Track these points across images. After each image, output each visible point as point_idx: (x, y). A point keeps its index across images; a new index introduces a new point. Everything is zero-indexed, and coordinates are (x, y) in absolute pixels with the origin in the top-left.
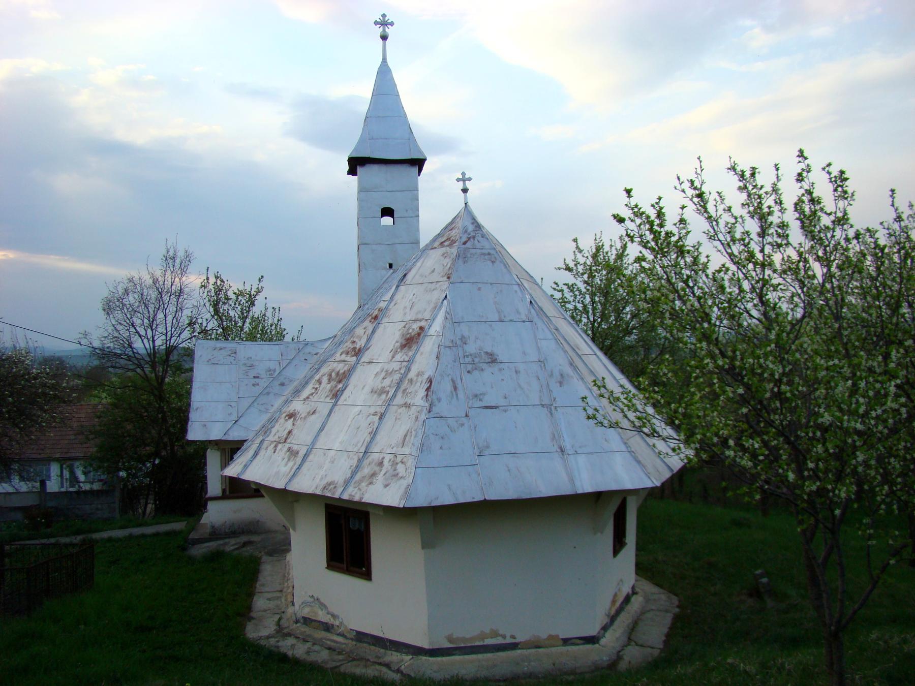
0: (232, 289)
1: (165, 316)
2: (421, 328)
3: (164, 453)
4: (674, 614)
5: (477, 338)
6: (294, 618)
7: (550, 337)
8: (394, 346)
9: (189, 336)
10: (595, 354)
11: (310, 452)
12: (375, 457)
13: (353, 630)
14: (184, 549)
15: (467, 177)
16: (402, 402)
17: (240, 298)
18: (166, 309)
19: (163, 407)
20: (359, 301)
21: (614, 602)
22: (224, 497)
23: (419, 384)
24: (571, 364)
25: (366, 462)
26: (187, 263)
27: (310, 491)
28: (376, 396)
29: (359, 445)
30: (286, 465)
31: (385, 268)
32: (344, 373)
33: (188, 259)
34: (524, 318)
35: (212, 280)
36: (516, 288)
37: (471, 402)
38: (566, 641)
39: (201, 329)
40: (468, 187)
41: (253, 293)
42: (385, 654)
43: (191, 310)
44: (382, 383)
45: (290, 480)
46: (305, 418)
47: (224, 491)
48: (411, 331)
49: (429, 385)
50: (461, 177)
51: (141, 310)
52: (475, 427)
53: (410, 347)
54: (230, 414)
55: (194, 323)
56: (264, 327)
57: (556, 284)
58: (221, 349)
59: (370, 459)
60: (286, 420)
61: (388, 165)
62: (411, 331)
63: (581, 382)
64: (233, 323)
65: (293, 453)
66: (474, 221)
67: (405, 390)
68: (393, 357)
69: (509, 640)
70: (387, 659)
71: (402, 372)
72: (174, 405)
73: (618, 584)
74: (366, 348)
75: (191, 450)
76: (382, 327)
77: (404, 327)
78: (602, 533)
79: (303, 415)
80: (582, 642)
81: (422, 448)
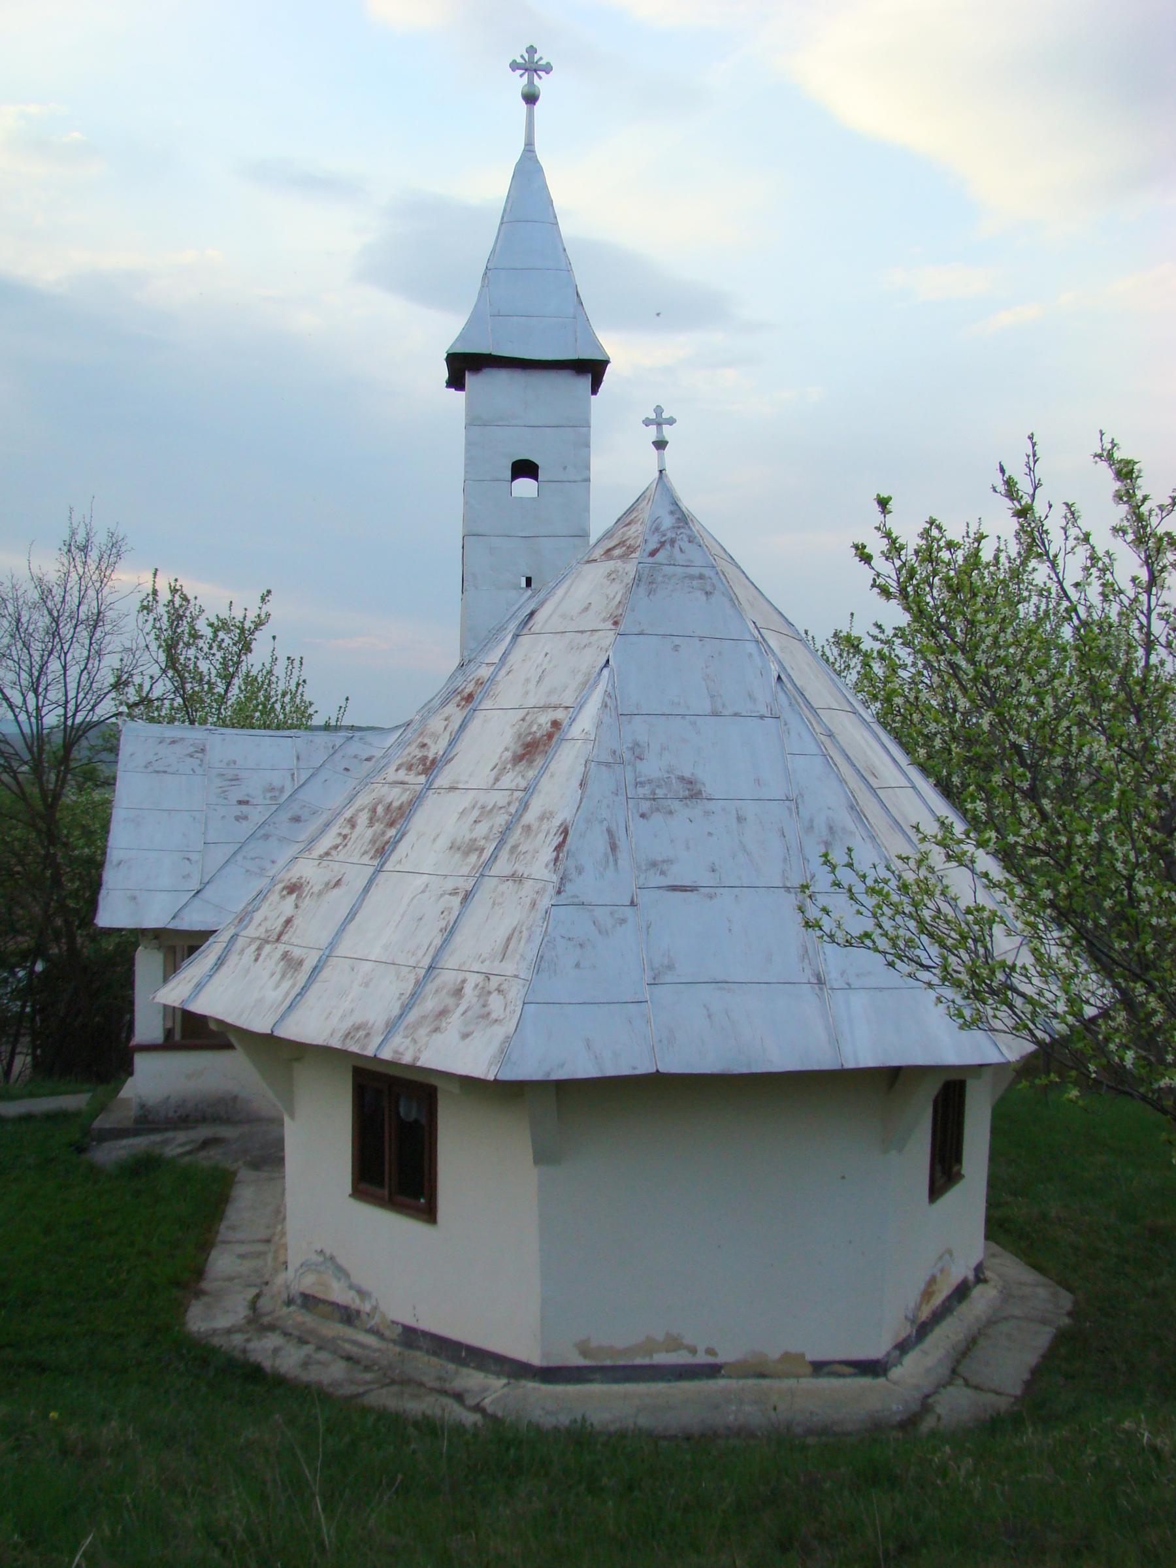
4: (1057, 1329)
5: (664, 748)
6: (285, 1296)
7: (815, 750)
8: (501, 757)
10: (914, 787)
11: (325, 962)
12: (448, 978)
13: (397, 1324)
14: (81, 1149)
16: (508, 871)
17: (221, 635)
18: (66, 654)
19: (55, 855)
20: (463, 647)
21: (927, 1294)
24: (852, 807)
25: (431, 987)
26: (112, 559)
27: (319, 1040)
28: (458, 856)
29: (420, 953)
30: (277, 986)
31: (517, 587)
32: (400, 807)
33: (114, 551)
34: (764, 711)
36: (751, 647)
37: (642, 877)
38: (819, 1368)
39: (140, 696)
40: (667, 439)
41: (248, 625)
43: (119, 656)
44: (471, 830)
45: (283, 1017)
46: (320, 894)
47: (169, 1033)
48: (534, 728)
49: (561, 839)
50: (653, 416)
51: (14, 653)
52: (648, 927)
53: (531, 762)
54: (187, 876)
55: (126, 683)
56: (268, 698)
57: (879, 627)
58: (173, 742)
59: (438, 981)
60: (283, 897)
61: (528, 371)
62: (534, 728)
63: (869, 845)
64: (206, 687)
65: (291, 963)
66: (675, 507)
67: (514, 848)
68: (497, 779)
69: (702, 1358)
70: (458, 1384)
71: (512, 809)
72: (76, 852)
74: (446, 758)
75: (109, 945)
76: (480, 716)
77: (523, 720)
79: (316, 889)
80: (851, 1370)
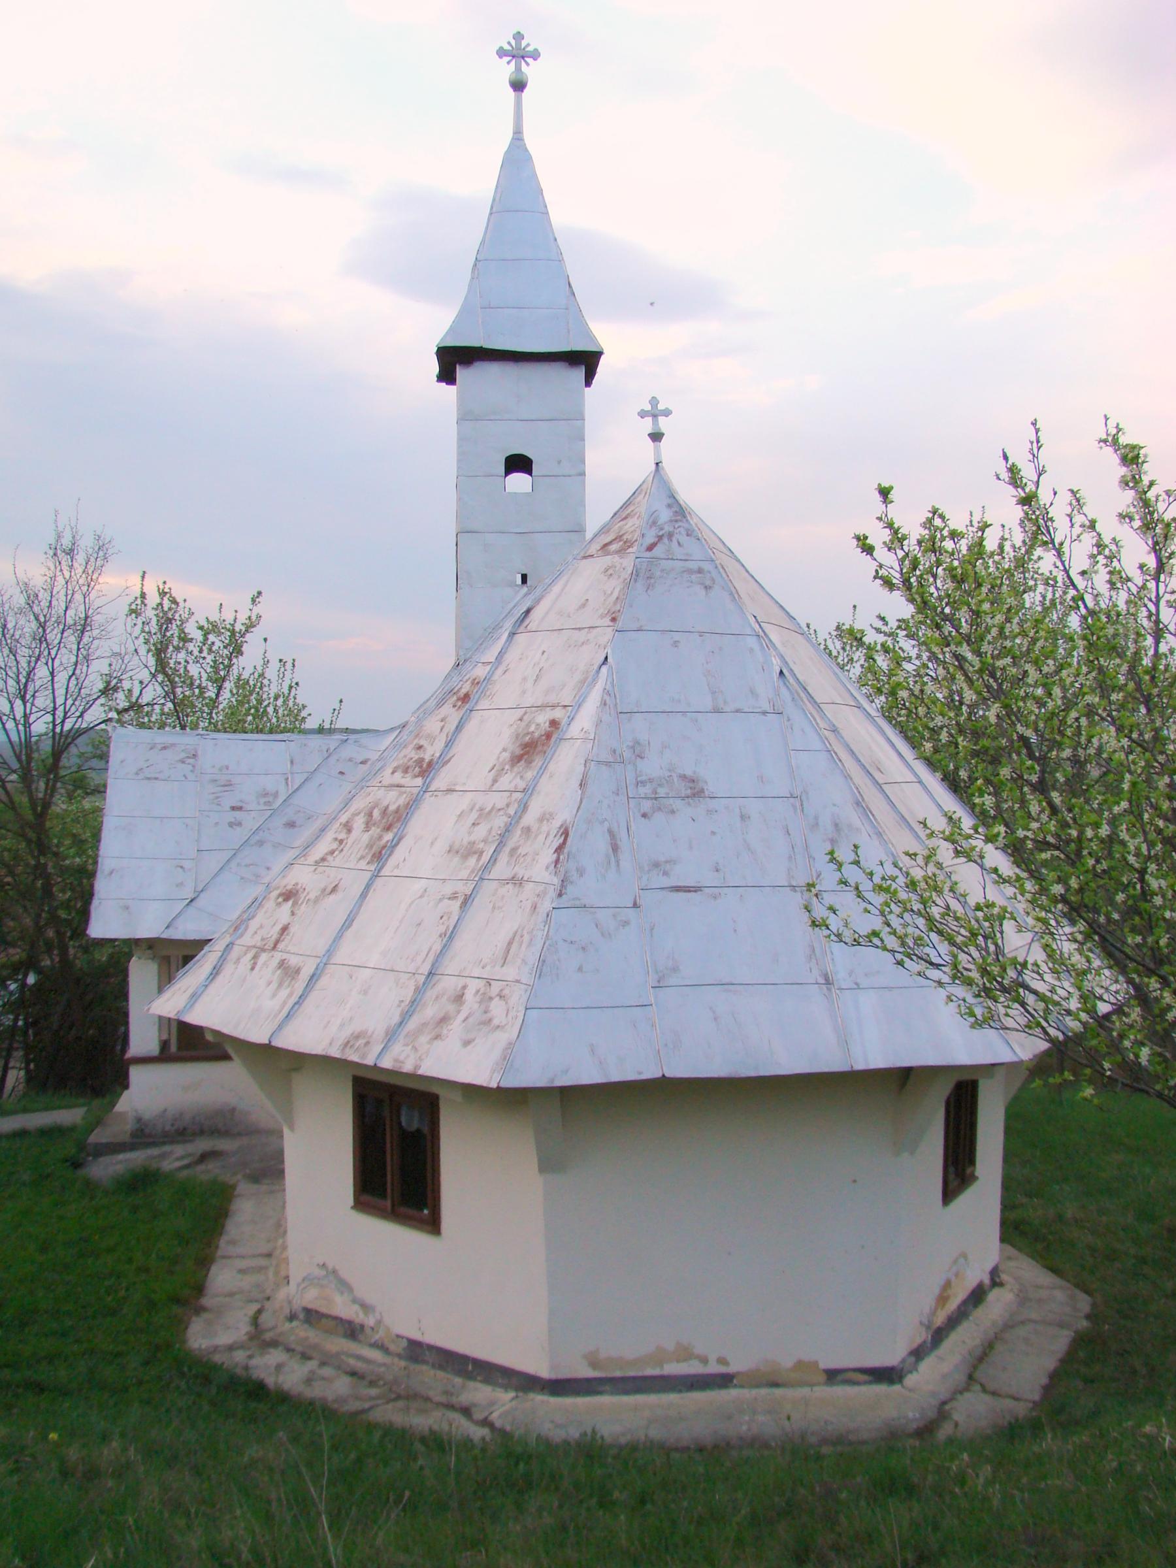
0: (193, 619)
1: (52, 674)
2: (554, 723)
3: (46, 962)
7: (818, 745)
8: (498, 758)
9: (103, 716)
10: (920, 782)
12: (447, 984)
14: (77, 1165)
15: (661, 407)
16: (508, 874)
17: (212, 638)
18: (53, 660)
19: (45, 865)
21: (942, 1299)
22: (165, 1056)
23: (541, 837)
24: (858, 804)
25: (431, 994)
26: (99, 562)
27: (318, 1050)
29: (420, 959)
30: (274, 995)
31: (512, 584)
32: (397, 811)
33: (101, 554)
34: (767, 707)
35: (153, 599)
36: (752, 642)
38: (833, 1376)
39: (129, 701)
40: (663, 430)
41: (238, 627)
42: (463, 1386)
43: (107, 661)
44: (470, 833)
45: (280, 1027)
46: (317, 900)
47: (164, 1045)
49: (561, 840)
50: (648, 408)
52: (652, 929)
53: (529, 762)
54: (180, 885)
55: (116, 689)
57: (883, 619)
58: (165, 748)
59: (439, 987)
60: (279, 904)
62: (532, 728)
64: (197, 691)
65: (288, 971)
67: (514, 850)
68: (495, 781)
69: (713, 1368)
70: (465, 1398)
71: (511, 811)
72: (67, 862)
73: (955, 1262)
75: (102, 956)
76: (476, 717)
77: (521, 720)
78: (912, 1153)
79: (312, 896)
81: (541, 968)
